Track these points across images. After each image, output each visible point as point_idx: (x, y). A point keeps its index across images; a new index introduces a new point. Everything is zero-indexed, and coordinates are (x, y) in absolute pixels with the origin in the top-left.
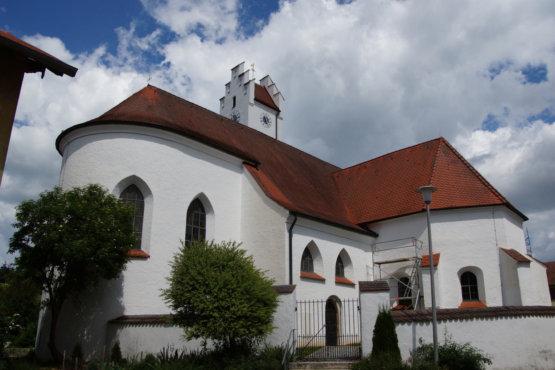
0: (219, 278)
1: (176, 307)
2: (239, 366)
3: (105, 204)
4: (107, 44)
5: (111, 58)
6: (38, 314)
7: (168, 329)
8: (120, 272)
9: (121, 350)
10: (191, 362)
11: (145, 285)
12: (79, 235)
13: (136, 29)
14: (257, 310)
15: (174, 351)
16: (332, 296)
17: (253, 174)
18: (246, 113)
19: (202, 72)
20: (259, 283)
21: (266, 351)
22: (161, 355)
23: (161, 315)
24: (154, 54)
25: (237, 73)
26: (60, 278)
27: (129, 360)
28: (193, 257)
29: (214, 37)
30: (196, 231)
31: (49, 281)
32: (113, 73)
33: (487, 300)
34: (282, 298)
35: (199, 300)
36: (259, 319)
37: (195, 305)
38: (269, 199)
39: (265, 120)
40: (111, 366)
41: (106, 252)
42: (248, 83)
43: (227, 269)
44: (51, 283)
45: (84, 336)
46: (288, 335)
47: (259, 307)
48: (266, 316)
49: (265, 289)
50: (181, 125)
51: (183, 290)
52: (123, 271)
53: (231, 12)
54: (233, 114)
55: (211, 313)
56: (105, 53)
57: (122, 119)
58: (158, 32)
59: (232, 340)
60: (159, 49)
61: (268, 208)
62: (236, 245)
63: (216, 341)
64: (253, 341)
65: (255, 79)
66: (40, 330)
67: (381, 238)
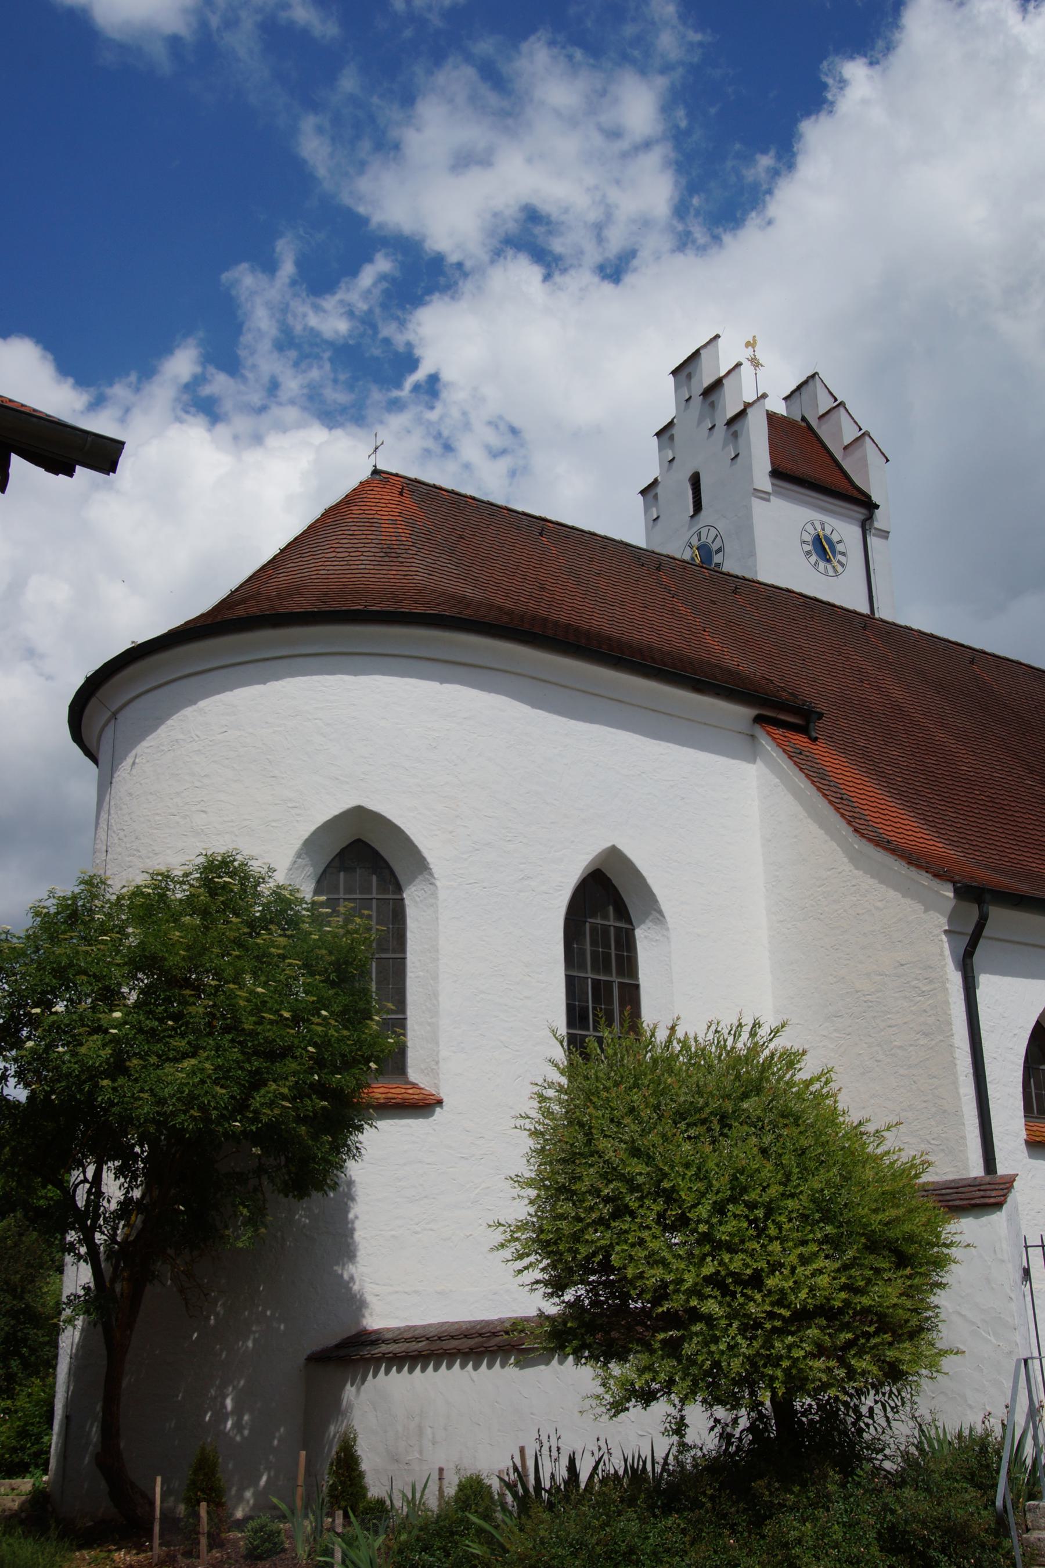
0: (711, 1165)
1: (557, 1286)
2: (820, 1513)
3: (265, 922)
4: (201, 334)
5: (220, 383)
6: (56, 1346)
7: (531, 1372)
8: (341, 1167)
9: (364, 1466)
10: (631, 1502)
11: (436, 1216)
12: (181, 1044)
13: (298, 264)
14: (869, 1281)
15: (564, 1462)
17: (795, 756)
18: (745, 528)
19: (561, 395)
20: (869, 1174)
21: (919, 1447)
22: (513, 1476)
23: (501, 1321)
24: (377, 352)
25: (694, 380)
26: (126, 1204)
27: (398, 1503)
28: (606, 1089)
29: (593, 255)
30: (601, 991)
31: (86, 1220)
32: (236, 438)
34: (964, 1228)
35: (643, 1254)
36: (882, 1317)
37: (630, 1272)
38: (870, 849)
39: (823, 548)
40: (332, 1529)
41: (284, 1097)
42: (742, 414)
43: (739, 1130)
44: (94, 1227)
45: (225, 1417)
46: (1008, 1385)
47: (877, 1271)
48: (909, 1304)
49: (892, 1198)
50: (509, 605)
51: (579, 1219)
52: (350, 1164)
53: (647, 145)
54: (695, 542)
55: (694, 1302)
56: (198, 370)
57: (293, 606)
58: (383, 264)
59: (783, 1407)
60: (388, 330)
61: (868, 882)
62: (764, 1032)
63: (720, 1412)
64: (864, 1410)
65: (764, 396)
66: (66, 1406)
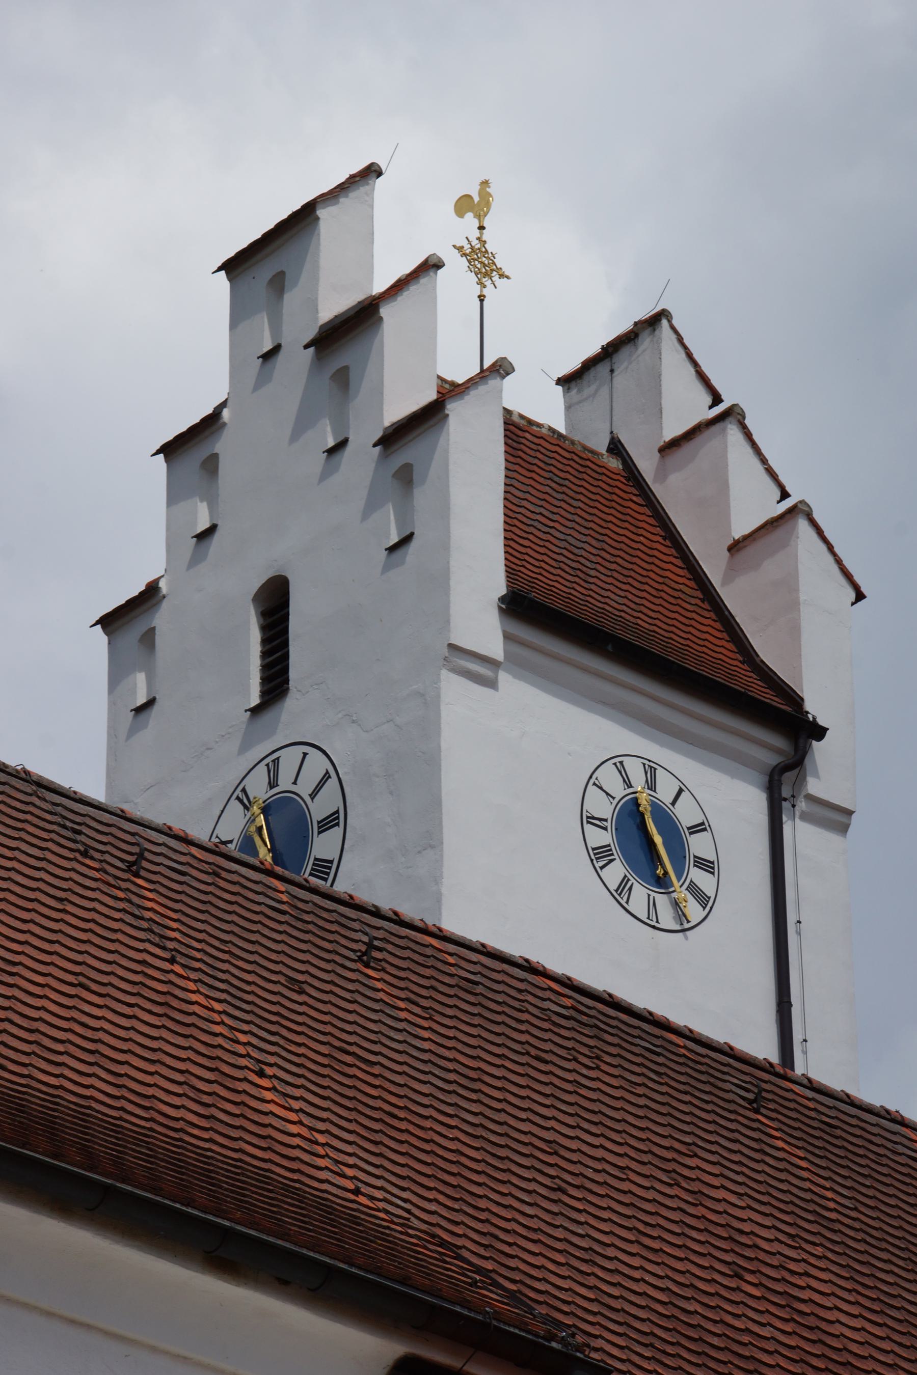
16: (502, 358)
18: (416, 763)
25: (292, 299)
42: (430, 416)
65: (501, 368)
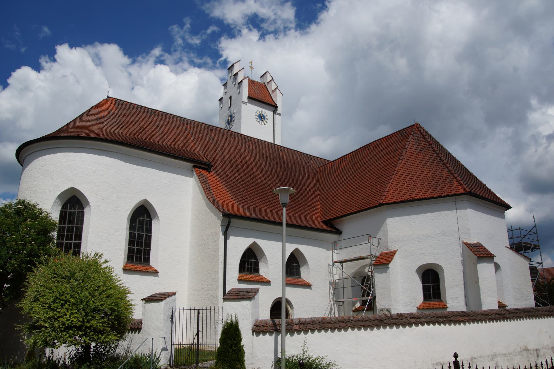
18: (240, 112)
33: (447, 299)
67: (344, 235)
